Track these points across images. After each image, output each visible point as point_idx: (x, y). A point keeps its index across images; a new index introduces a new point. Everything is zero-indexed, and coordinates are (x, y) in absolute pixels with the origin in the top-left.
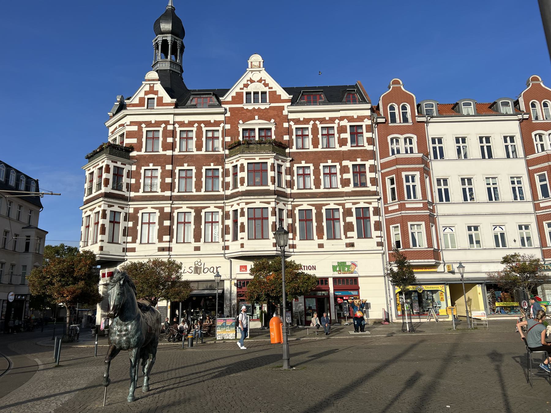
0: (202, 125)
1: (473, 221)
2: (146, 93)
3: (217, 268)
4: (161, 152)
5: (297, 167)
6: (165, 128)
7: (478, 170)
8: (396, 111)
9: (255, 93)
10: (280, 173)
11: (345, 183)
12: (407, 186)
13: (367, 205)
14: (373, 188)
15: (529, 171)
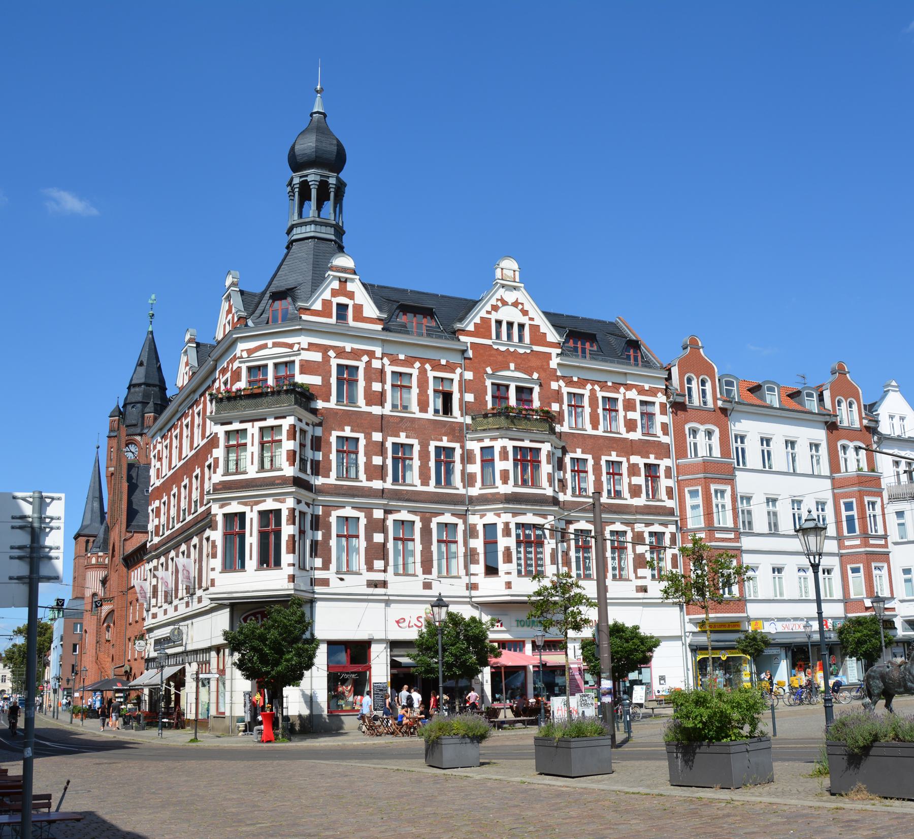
1: (778, 560)
2: (335, 293)
6: (369, 363)
11: (635, 491)
15: (834, 495)
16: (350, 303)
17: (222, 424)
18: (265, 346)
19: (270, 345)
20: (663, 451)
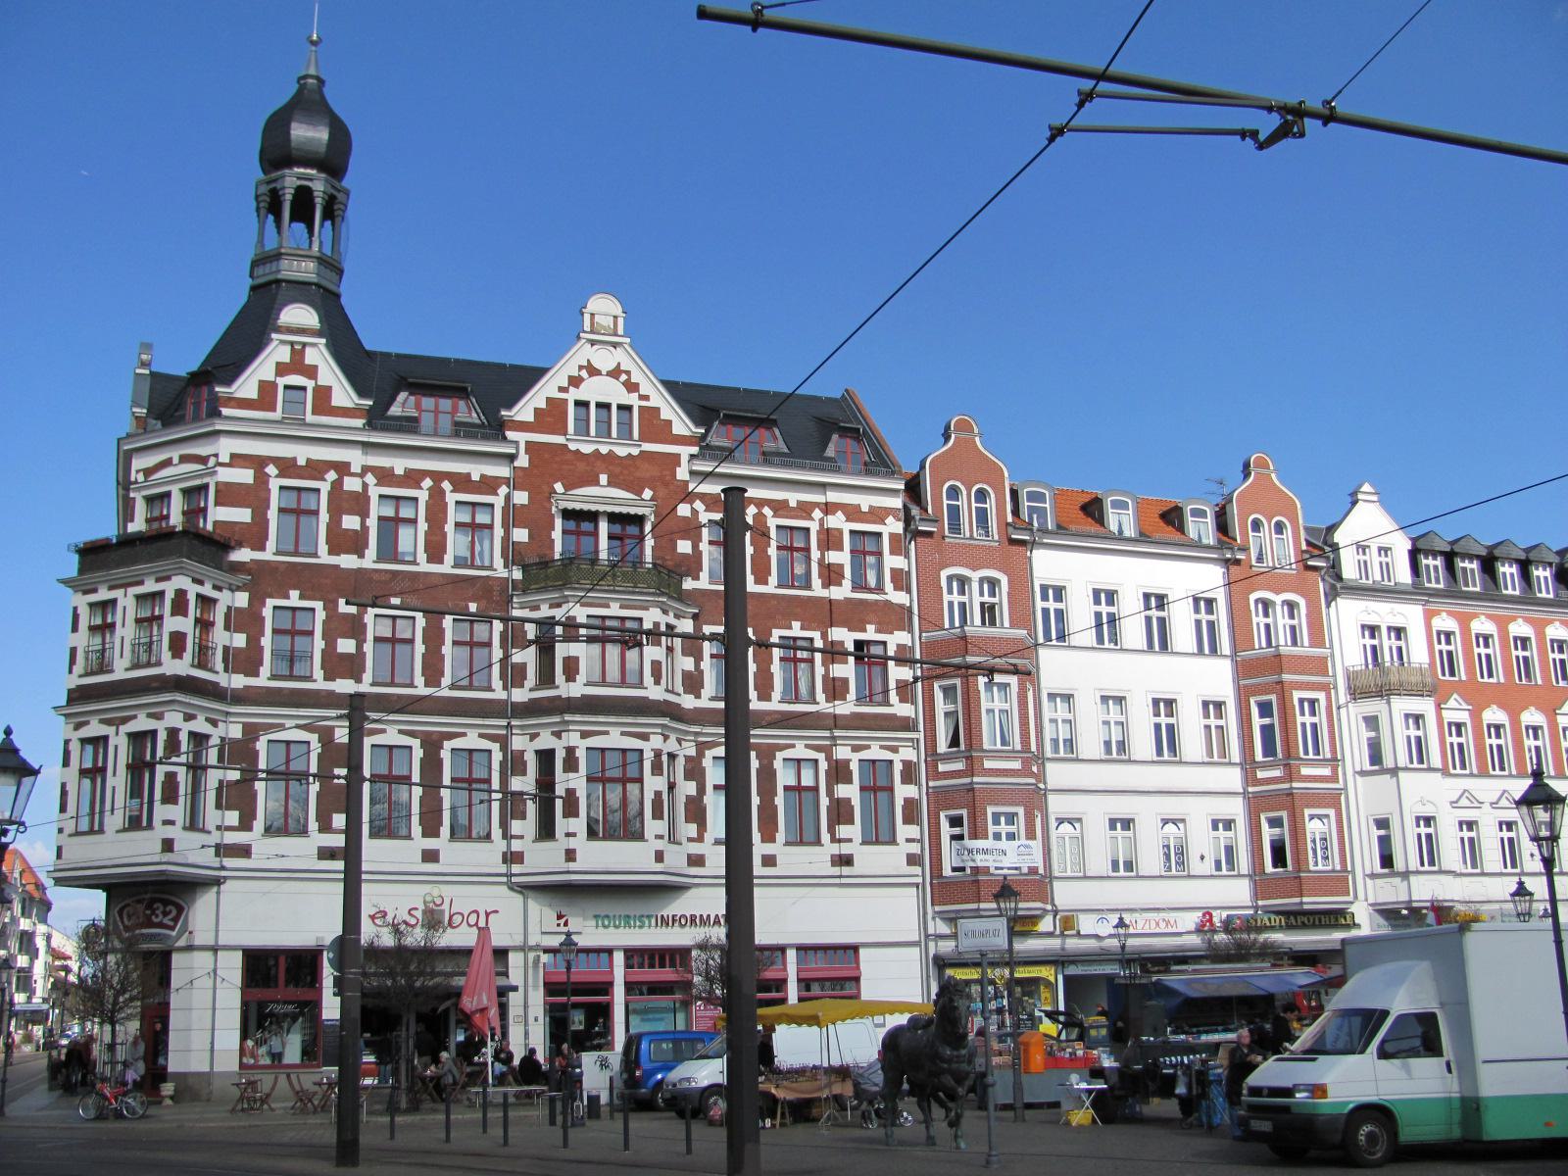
0: (446, 485)
1: (1122, 807)
2: (282, 369)
3: (487, 915)
4: (324, 557)
5: (275, 607)
6: (337, 485)
7: (1141, 675)
8: (962, 502)
9: (599, 405)
10: (204, 625)
12: (1263, 728)
13: (887, 755)
14: (904, 710)
17: (86, 592)
18: (167, 463)
19: (176, 460)
20: (895, 618)
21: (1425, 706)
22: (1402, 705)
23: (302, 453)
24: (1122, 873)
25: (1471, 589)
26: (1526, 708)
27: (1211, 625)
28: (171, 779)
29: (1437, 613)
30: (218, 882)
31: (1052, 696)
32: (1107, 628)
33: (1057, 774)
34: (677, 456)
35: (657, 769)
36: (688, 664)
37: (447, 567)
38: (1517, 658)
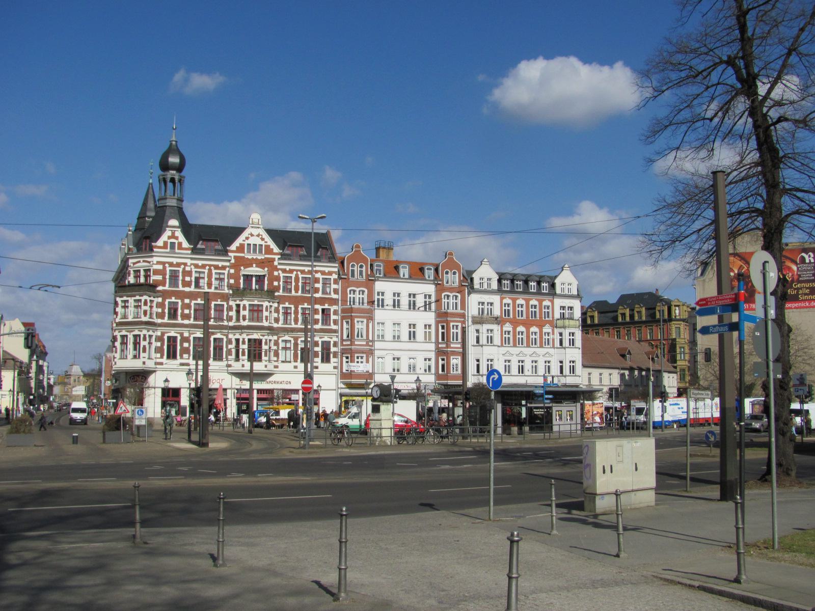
0: (212, 268)
2: (169, 238)
6: (184, 269)
7: (406, 317)
8: (355, 269)
10: (151, 307)
13: (329, 340)
14: (333, 327)
16: (176, 242)
18: (139, 262)
20: (333, 302)
21: (496, 328)
22: (486, 326)
23: (175, 261)
24: (427, 372)
25: (519, 290)
26: (519, 326)
27: (456, 303)
28: (144, 347)
29: (505, 298)
30: (155, 371)
31: (378, 323)
32: (396, 304)
33: (378, 345)
34: (275, 258)
35: (266, 344)
36: (276, 315)
37: (212, 290)
38: (532, 311)
